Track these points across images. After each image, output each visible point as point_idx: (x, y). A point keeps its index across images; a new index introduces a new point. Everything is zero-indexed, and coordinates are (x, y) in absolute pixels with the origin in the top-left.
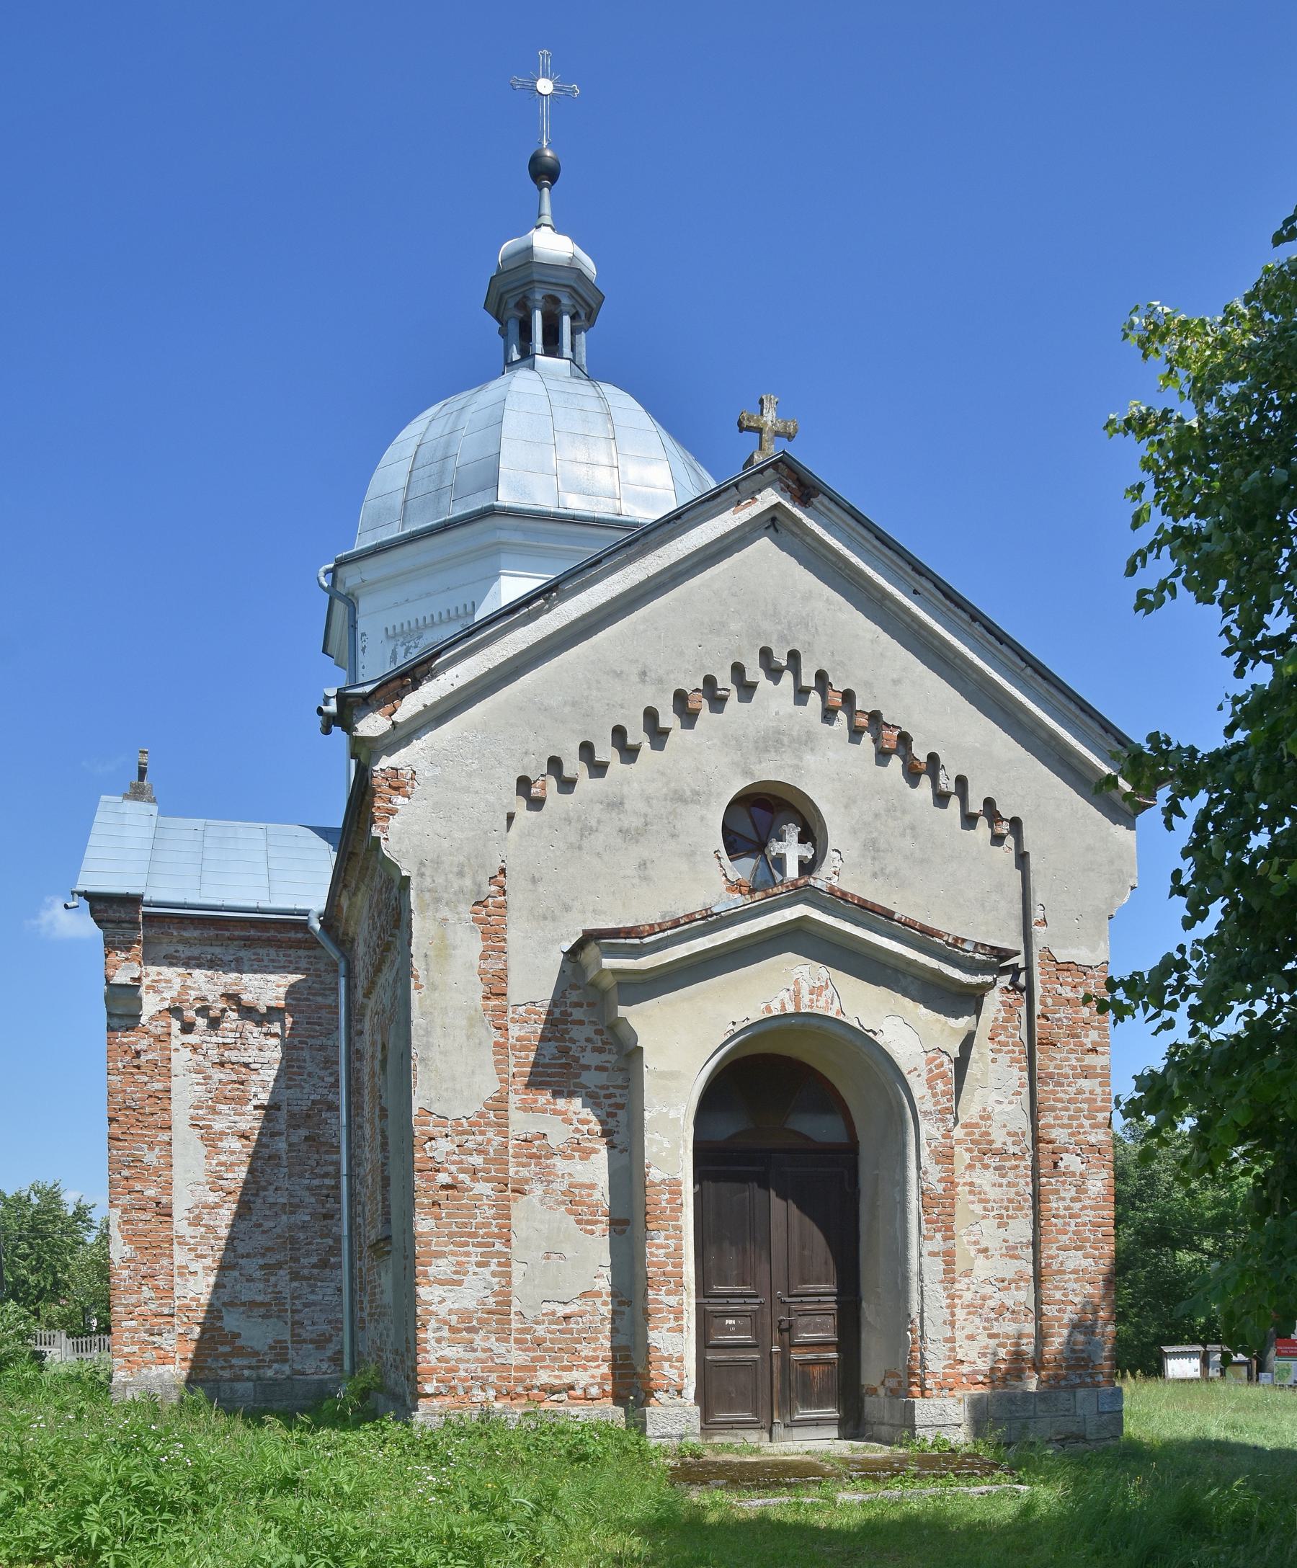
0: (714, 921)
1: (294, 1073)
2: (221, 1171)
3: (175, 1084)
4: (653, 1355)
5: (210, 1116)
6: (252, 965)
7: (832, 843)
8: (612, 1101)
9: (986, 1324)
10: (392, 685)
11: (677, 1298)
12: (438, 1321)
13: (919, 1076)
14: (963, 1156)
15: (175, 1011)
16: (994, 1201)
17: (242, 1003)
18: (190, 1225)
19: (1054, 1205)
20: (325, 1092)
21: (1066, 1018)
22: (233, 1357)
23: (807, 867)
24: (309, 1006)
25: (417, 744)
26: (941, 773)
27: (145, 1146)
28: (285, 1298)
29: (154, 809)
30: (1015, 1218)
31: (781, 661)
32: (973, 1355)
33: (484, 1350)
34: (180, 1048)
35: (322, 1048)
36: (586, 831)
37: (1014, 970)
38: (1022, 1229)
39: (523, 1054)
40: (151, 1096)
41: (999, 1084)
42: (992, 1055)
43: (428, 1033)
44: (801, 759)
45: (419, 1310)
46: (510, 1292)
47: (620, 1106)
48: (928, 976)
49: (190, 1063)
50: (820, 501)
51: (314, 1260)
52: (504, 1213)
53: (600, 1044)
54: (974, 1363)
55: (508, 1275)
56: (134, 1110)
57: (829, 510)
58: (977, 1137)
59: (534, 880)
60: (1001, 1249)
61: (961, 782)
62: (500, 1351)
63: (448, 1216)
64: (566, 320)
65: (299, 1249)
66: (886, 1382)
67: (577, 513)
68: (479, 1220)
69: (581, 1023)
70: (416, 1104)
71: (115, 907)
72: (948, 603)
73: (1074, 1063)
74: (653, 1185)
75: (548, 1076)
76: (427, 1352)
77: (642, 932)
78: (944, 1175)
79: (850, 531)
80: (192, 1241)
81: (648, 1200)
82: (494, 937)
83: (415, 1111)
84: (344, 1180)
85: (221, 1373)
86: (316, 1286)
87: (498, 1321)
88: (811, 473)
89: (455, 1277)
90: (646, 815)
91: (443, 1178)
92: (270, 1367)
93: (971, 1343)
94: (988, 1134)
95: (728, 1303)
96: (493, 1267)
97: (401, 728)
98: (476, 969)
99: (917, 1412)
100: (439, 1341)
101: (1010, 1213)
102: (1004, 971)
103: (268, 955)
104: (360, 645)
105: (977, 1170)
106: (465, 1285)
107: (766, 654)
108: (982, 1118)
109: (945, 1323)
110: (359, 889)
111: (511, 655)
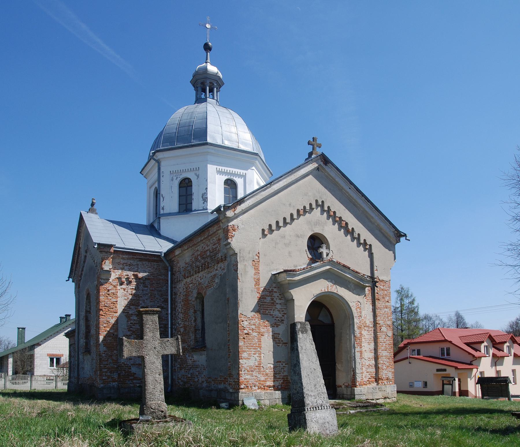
1: (152, 298)
3: (119, 300)
8: (283, 312)
10: (235, 204)
15: (119, 279)
19: (380, 339)
20: (161, 303)
22: (134, 380)
25: (239, 219)
26: (354, 233)
27: (110, 318)
33: (255, 376)
34: (120, 289)
36: (276, 243)
39: (263, 300)
40: (112, 303)
42: (366, 302)
43: (242, 293)
44: (324, 227)
45: (240, 366)
47: (285, 314)
48: (356, 283)
49: (123, 294)
55: (260, 357)
56: (107, 307)
57: (331, 167)
58: (363, 322)
59: (265, 255)
61: (359, 235)
64: (215, 89)
66: (345, 384)
67: (229, 146)
69: (276, 292)
70: (239, 312)
71: (106, 248)
73: (384, 305)
75: (269, 305)
76: (242, 377)
82: (257, 269)
83: (239, 314)
85: (130, 385)
87: (258, 369)
89: (249, 357)
91: (246, 331)
94: (366, 322)
96: (257, 355)
99: (355, 391)
100: (244, 374)
103: (146, 264)
104: (161, 175)
106: (251, 359)
107: (317, 201)
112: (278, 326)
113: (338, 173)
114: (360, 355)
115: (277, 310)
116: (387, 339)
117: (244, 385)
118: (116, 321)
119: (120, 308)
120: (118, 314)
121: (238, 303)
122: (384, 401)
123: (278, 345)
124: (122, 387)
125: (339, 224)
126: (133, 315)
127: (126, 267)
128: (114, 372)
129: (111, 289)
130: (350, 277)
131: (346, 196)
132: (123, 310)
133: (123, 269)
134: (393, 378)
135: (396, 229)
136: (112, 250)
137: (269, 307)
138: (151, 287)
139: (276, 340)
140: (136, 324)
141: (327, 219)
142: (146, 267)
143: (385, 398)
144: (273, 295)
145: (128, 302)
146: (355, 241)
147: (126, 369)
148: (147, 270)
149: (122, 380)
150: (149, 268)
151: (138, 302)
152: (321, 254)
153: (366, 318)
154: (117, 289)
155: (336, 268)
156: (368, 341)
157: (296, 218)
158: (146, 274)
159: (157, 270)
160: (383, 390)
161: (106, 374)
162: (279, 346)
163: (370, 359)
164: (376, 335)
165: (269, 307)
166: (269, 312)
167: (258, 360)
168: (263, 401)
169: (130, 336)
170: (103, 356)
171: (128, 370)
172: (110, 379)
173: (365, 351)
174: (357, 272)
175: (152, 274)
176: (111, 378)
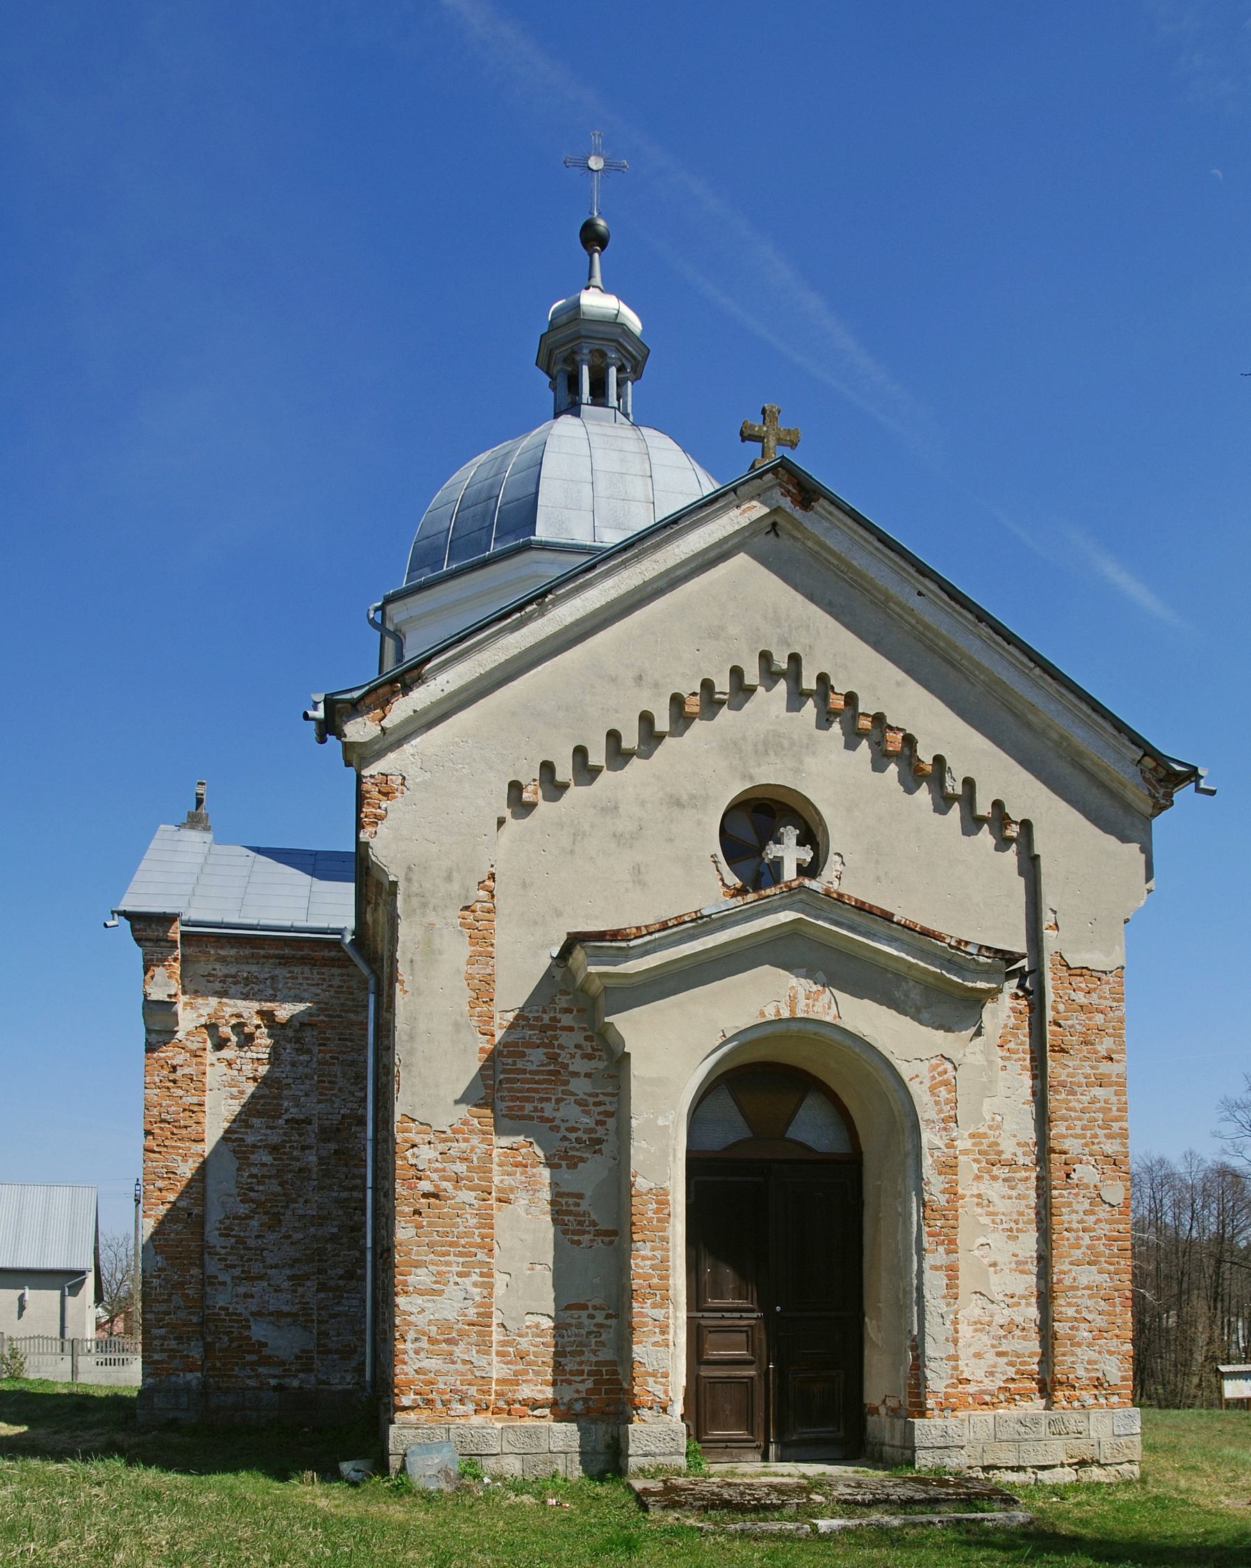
0: (702, 924)
1: (326, 1088)
2: (251, 1183)
3: (208, 1099)
4: (638, 1371)
5: (242, 1130)
6: (287, 983)
7: (833, 847)
8: (601, 1108)
9: (995, 1342)
10: (381, 691)
11: (663, 1311)
12: (417, 1332)
13: (921, 1083)
14: (968, 1166)
15: (211, 1028)
16: (1003, 1214)
17: (277, 1019)
18: (221, 1235)
20: (355, 1106)
21: (1080, 1024)
23: (810, 870)
24: (341, 1023)
25: (408, 748)
27: (179, 1158)
28: (312, 1309)
29: (208, 837)
30: (1025, 1232)
31: (781, 664)
32: (980, 1374)
33: (465, 1362)
34: (216, 1062)
35: (353, 1063)
36: (578, 835)
37: (1021, 973)
38: (1029, 1243)
39: (510, 1061)
40: (185, 1110)
41: (1009, 1093)
42: (1001, 1063)
43: (412, 1038)
44: (801, 762)
45: (398, 1321)
46: (492, 1303)
48: (931, 980)
49: (224, 1078)
50: (821, 505)
51: (340, 1271)
52: (486, 1221)
53: (590, 1051)
54: (981, 1382)
55: (491, 1286)
56: (169, 1123)
57: (830, 513)
58: (984, 1147)
59: (524, 885)
60: (1010, 1263)
61: (969, 783)
62: (481, 1364)
63: (430, 1224)
64: (613, 371)
65: (326, 1261)
66: (887, 1401)
68: (462, 1229)
69: (571, 1029)
71: (153, 926)
72: (953, 603)
73: (1089, 1071)
74: (640, 1195)
75: (536, 1082)
76: (405, 1363)
77: (630, 934)
78: (947, 1186)
79: (851, 534)
80: (223, 1251)
81: (634, 1210)
82: (481, 939)
83: (397, 1117)
84: (369, 1192)
85: (248, 1381)
86: (342, 1297)
87: (479, 1334)
88: (810, 477)
89: (435, 1286)
90: (640, 819)
91: (425, 1186)
92: (295, 1377)
93: (977, 1361)
94: (997, 1144)
95: (723, 1317)
96: (475, 1278)
97: (391, 734)
98: (463, 975)
100: (417, 1352)
101: (1020, 1226)
102: (1010, 976)
105: (985, 1181)
106: (445, 1296)
107: (765, 657)
108: (990, 1127)
109: (947, 1339)
110: (379, 904)
111: (503, 660)
112: (575, 1166)
113: (861, 536)
114: (945, 1281)
115: (572, 1098)
116: (1102, 1215)
117: (412, 1396)
118: (199, 1169)
119: (214, 1129)
120: (207, 1148)
121: (394, 1077)
122: (1074, 1477)
123: (576, 1238)
124: (219, 1388)
125: (878, 744)
126: (260, 1147)
127: (233, 990)
128: (189, 1339)
129: (181, 1062)
130: (895, 953)
131: (907, 627)
132: (227, 1132)
133: (222, 994)
134: (1124, 1379)
135: (1149, 751)
136: (175, 932)
137: (536, 1091)
138: (320, 1052)
139: (566, 1218)
140: (270, 1177)
141: (819, 727)
142: (305, 987)
143: (1082, 1463)
144: (556, 1043)
145: (243, 1106)
146: (956, 811)
147: (232, 1327)
148: (306, 995)
149: (218, 1364)
150: (313, 989)
151: (278, 1105)
152: (778, 863)
153: (999, 1127)
154: (202, 1064)
155: (825, 919)
156: (1005, 1226)
157: (667, 729)
158: (301, 1007)
159: (342, 992)
160: (1072, 1428)
161: (162, 1345)
162: (579, 1243)
163: (1015, 1300)
164: (1045, 1202)
165: (536, 1091)
166: (536, 1110)
167: (477, 1298)
168: (493, 1459)
169: (248, 1217)
170: (153, 1285)
171: (240, 1333)
172: (177, 1361)
173: (994, 1265)
174: (925, 933)
175: (322, 1007)
176: (182, 1357)
